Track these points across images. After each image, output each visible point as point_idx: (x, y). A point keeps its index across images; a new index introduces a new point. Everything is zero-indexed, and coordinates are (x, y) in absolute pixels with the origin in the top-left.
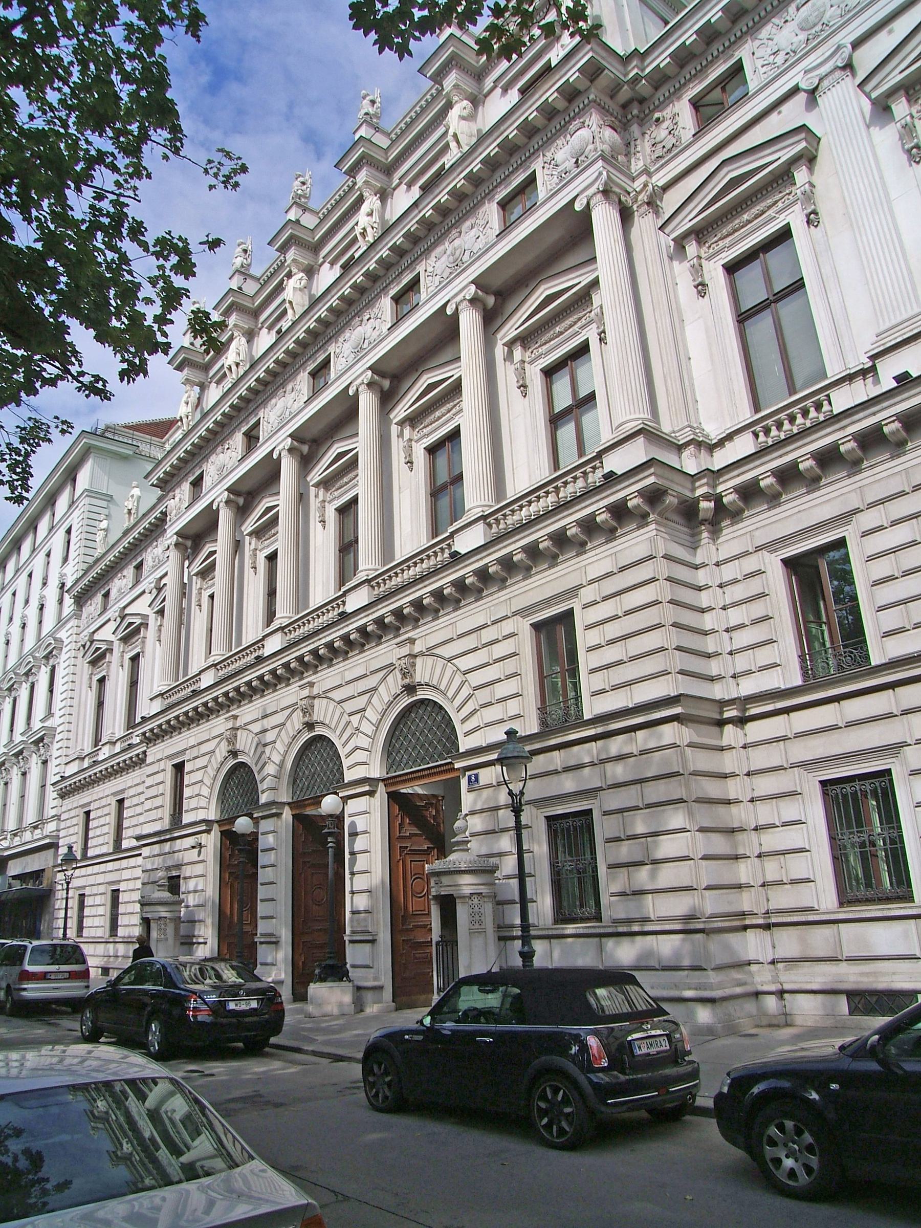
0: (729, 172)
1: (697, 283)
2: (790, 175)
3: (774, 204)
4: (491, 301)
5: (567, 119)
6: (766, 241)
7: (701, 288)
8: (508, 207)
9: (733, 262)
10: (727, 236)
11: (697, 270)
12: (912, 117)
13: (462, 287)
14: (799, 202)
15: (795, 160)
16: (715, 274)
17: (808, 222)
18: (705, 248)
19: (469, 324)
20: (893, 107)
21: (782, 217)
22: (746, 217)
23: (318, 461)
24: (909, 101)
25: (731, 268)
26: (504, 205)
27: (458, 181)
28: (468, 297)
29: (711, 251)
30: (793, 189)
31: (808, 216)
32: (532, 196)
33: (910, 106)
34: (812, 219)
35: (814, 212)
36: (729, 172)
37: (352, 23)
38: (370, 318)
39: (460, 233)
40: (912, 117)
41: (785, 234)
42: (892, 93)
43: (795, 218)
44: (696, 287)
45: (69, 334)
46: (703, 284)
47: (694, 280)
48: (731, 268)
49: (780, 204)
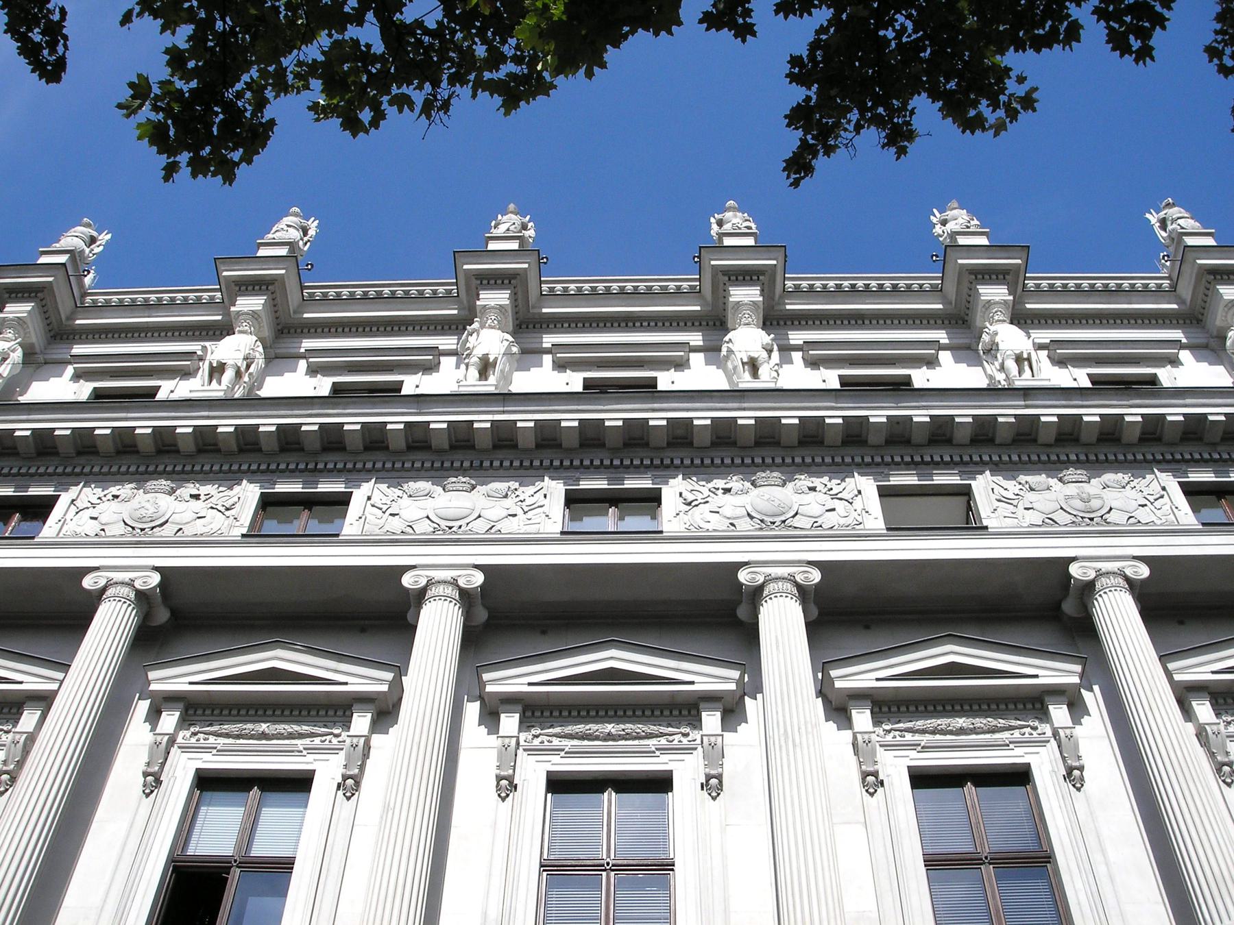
0: (612, 658)
1: (150, 770)
2: (348, 713)
3: (657, 736)
4: (162, 616)
5: (263, 467)
6: (262, 775)
7: (153, 781)
8: (270, 509)
9: (1002, 770)
10: (227, 736)
11: (508, 756)
12: (518, 743)
13: (142, 567)
14: (342, 754)
15: (711, 699)
16: (533, 774)
17: (339, 786)
18: (188, 734)
19: (111, 627)
20: (503, 716)
21: (310, 758)
22: (264, 727)
23: (340, 658)
24: (521, 722)
25: (208, 782)
26: (268, 503)
27: (395, 420)
28: (138, 585)
29: (193, 740)
30: (344, 734)
31: (709, 777)
32: (337, 521)
33: (520, 731)
34: (350, 785)
35: (719, 777)
36: (612, 658)
37: (798, 94)
38: (96, 519)
39: (473, 487)
40: (518, 743)
41: (661, 783)
42: (860, 696)
43: (327, 771)
44: (146, 774)
45: (528, 103)
46: (510, 779)
47: (148, 764)
48: (208, 782)
49: (317, 740)
